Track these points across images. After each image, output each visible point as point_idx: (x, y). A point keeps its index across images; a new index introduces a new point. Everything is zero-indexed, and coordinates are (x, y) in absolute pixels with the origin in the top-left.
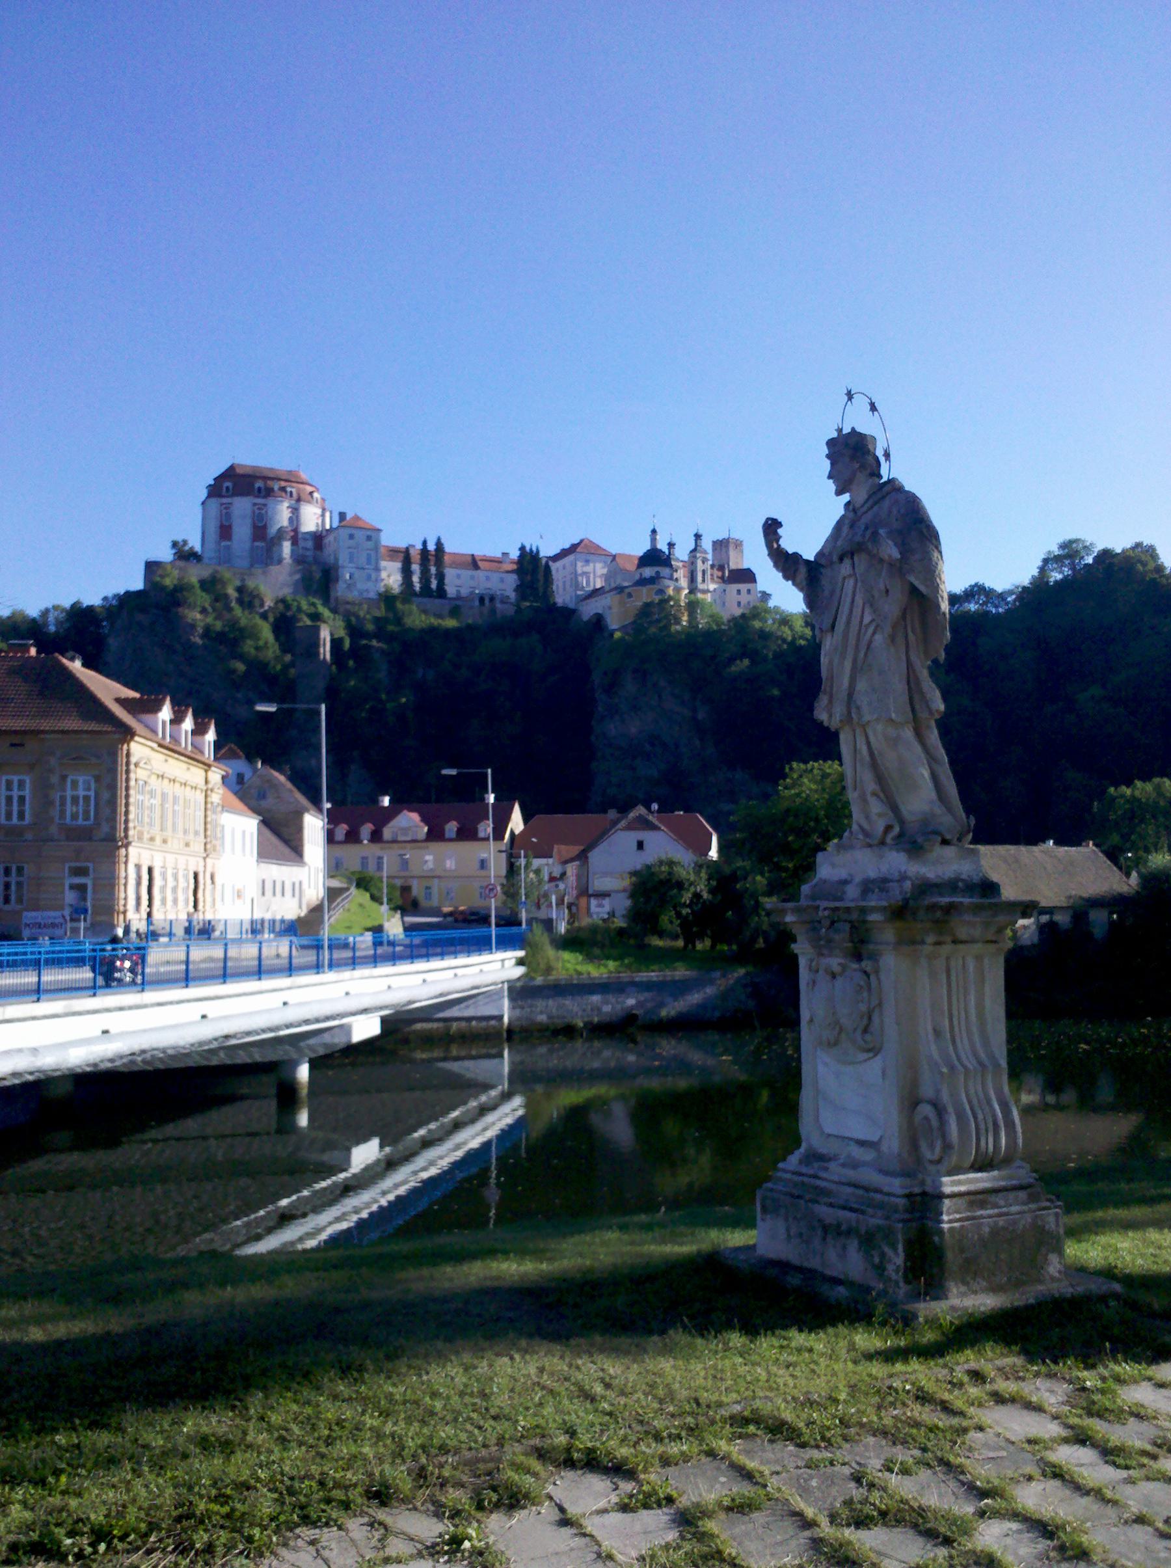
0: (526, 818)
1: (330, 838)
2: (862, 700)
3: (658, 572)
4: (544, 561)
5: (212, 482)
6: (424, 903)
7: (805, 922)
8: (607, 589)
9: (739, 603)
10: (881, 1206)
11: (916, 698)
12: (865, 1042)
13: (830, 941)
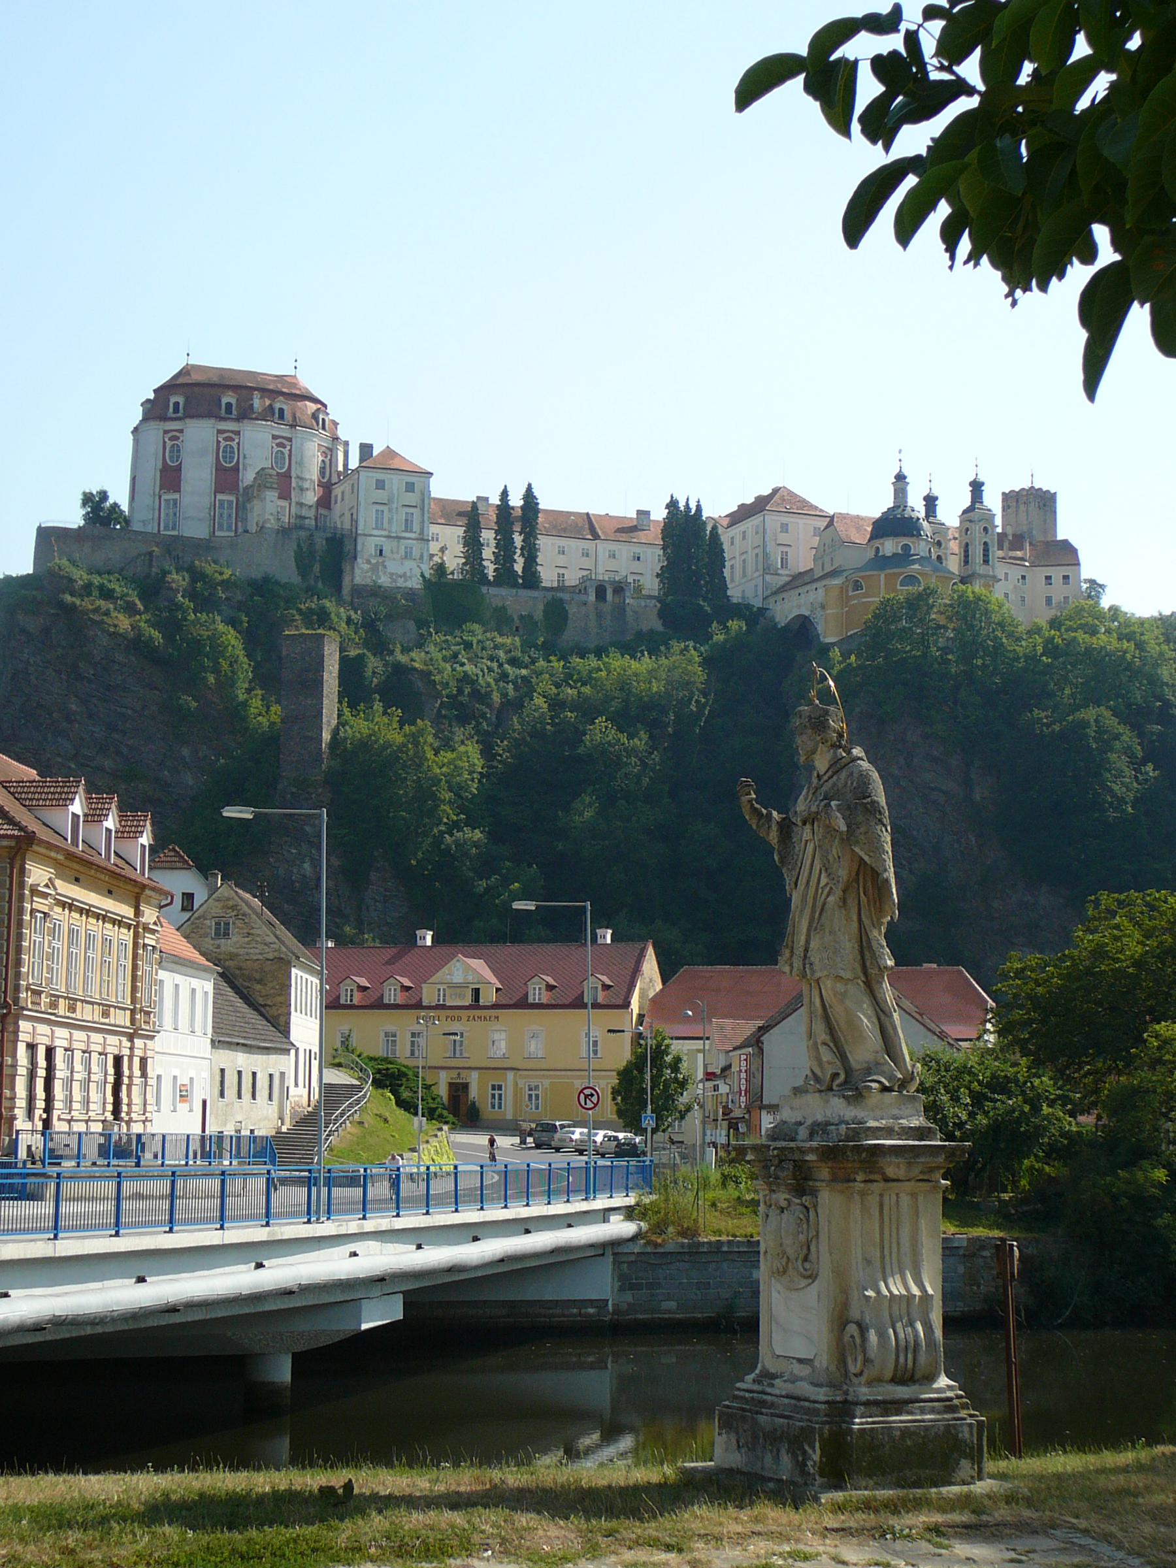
0: (666, 974)
1: (332, 1004)
2: (814, 957)
3: (906, 547)
4: (709, 528)
5: (152, 396)
6: (487, 1112)
7: (760, 1161)
8: (818, 573)
9: (1049, 600)
10: (808, 1411)
11: (867, 955)
12: (806, 1270)
13: (777, 1178)
